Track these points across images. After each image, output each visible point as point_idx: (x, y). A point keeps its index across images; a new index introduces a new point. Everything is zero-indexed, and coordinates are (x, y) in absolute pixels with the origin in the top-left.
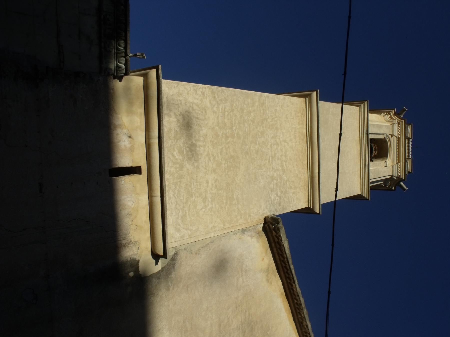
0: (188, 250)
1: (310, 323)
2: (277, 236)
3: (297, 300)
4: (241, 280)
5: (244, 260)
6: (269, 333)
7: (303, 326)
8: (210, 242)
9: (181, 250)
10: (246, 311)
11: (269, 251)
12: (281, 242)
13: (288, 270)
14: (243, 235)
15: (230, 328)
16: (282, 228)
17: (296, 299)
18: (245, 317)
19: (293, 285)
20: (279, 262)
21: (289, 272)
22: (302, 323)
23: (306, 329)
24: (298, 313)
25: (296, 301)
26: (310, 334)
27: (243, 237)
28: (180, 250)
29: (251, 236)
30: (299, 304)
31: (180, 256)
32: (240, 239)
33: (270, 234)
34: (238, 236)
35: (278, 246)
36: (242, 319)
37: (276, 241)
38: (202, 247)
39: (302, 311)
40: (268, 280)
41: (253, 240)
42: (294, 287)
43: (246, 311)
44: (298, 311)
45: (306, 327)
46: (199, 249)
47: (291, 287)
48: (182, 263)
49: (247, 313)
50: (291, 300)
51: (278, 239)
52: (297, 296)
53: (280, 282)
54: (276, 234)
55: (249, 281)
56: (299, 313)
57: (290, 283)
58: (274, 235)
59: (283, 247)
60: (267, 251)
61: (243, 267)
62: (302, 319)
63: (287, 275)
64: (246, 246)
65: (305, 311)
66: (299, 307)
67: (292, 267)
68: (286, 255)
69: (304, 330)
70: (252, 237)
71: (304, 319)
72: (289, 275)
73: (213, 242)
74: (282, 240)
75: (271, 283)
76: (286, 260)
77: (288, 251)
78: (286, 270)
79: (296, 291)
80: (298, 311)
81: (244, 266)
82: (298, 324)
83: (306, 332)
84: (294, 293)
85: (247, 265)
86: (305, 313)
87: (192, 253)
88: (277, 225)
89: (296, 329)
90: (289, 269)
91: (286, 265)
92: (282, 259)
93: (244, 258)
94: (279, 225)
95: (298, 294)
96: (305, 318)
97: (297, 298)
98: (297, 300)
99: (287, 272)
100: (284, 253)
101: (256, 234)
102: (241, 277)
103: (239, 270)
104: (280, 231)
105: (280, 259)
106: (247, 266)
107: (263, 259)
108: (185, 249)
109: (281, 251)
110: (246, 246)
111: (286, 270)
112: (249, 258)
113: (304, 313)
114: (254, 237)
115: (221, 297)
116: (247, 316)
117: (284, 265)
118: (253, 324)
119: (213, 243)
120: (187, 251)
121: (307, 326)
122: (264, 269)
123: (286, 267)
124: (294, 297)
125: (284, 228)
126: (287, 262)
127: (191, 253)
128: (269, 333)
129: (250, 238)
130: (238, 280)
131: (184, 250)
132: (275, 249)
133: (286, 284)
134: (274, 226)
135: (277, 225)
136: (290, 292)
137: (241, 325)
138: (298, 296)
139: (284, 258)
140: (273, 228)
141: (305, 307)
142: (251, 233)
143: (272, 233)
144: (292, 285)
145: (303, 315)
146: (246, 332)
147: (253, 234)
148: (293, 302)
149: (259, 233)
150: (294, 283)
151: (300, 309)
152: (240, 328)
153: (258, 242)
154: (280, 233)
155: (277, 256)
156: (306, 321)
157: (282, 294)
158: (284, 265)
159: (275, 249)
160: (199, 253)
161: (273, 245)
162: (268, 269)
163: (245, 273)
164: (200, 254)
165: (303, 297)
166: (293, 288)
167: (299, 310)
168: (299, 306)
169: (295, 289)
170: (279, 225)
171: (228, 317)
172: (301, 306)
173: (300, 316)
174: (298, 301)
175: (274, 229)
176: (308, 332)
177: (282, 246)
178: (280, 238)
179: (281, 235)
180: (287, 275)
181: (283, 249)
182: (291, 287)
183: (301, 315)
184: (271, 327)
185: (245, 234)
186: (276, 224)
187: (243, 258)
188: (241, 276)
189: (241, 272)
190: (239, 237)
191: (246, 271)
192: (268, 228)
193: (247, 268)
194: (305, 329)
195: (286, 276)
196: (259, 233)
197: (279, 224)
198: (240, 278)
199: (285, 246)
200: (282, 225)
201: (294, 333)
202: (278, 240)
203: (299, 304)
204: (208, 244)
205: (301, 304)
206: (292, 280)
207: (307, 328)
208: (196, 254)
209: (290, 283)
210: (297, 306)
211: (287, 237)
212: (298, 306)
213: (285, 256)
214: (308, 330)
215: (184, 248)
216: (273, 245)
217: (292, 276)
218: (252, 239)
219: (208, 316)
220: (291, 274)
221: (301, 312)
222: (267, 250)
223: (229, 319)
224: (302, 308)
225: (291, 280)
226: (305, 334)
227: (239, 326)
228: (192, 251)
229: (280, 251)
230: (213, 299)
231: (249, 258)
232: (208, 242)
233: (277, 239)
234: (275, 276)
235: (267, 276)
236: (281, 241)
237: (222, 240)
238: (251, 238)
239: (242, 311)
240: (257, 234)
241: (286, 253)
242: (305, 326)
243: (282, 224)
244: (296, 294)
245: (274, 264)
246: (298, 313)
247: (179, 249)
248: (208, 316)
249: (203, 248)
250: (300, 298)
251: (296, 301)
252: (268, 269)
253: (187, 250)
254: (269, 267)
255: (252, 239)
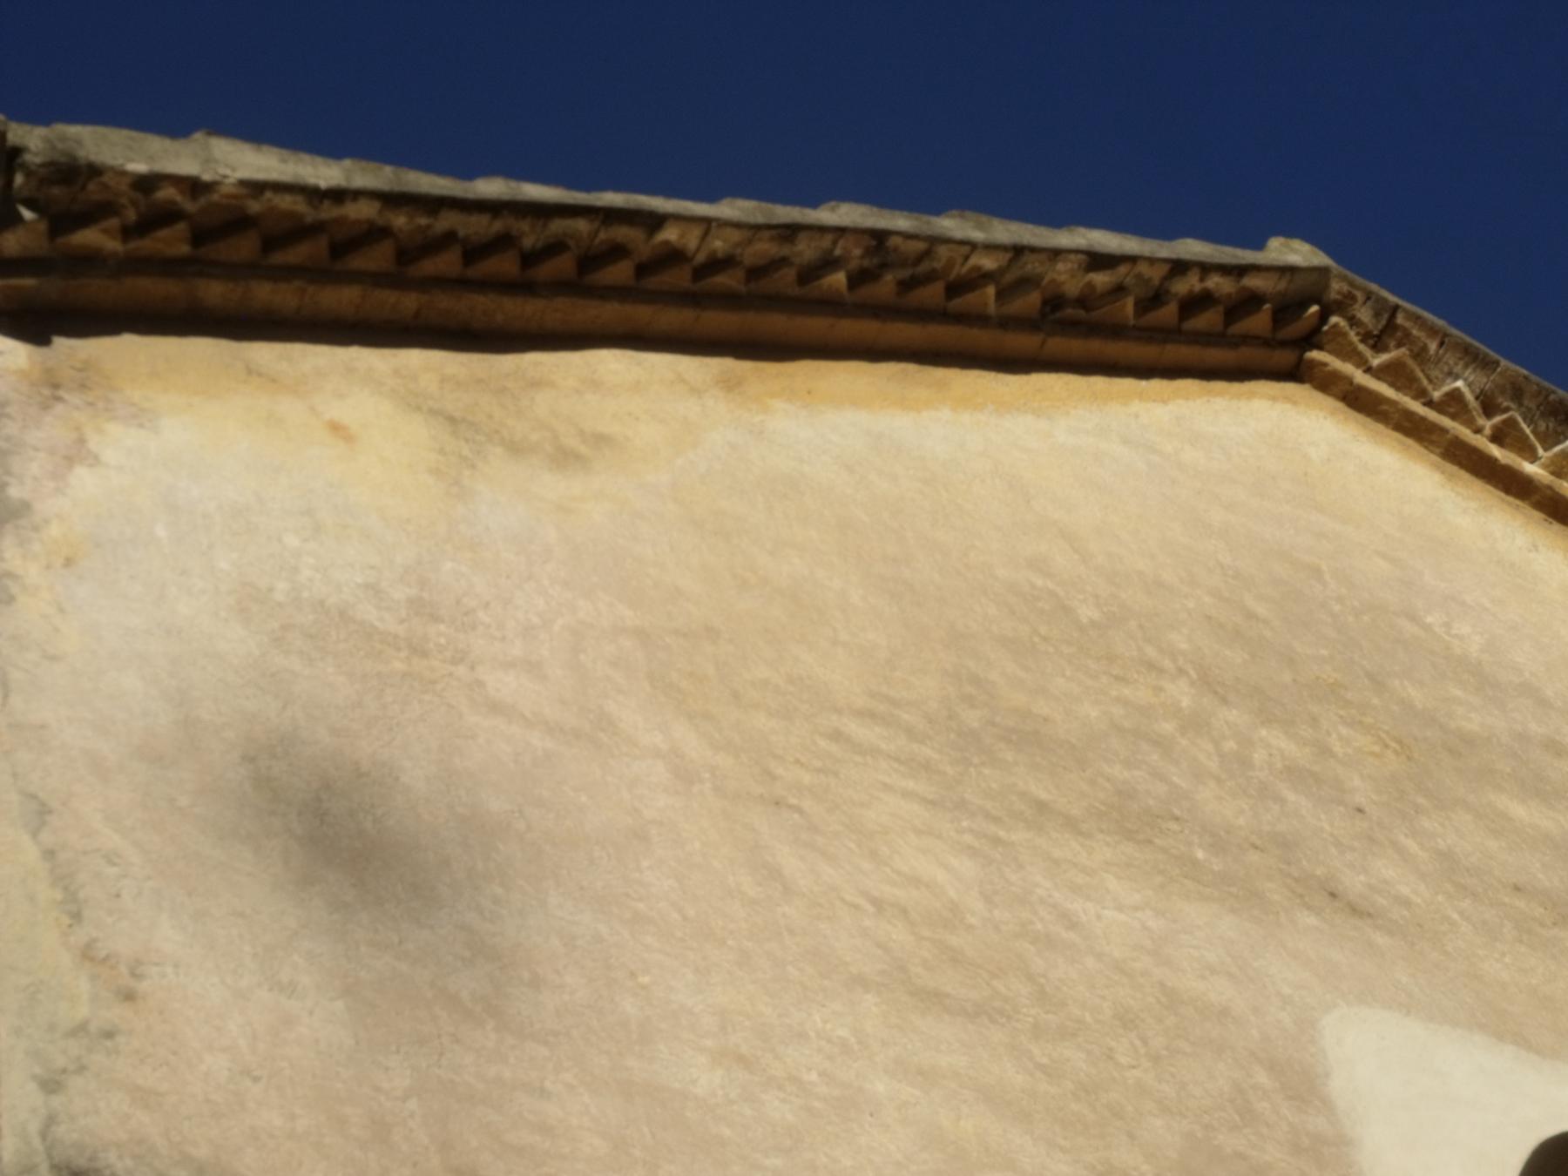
0: (61, 1062)
1: (1082, 230)
2: (131, 215)
3: (829, 263)
4: (504, 685)
5: (305, 594)
6: (1087, 613)
7: (1085, 300)
8: (35, 834)
9: (51, 1120)
10: (837, 736)
11: (264, 353)
12: (215, 197)
13: (504, 241)
14: (36, 529)
15: (972, 920)
16: (63, 139)
17: (809, 274)
18: (897, 760)
19: (667, 243)
20: (408, 303)
21: (530, 235)
22: (1055, 302)
23: (1128, 281)
24: (958, 304)
25: (838, 279)
26: (1179, 267)
27: (55, 530)
28: (44, 1135)
29: (70, 461)
30: (866, 263)
31: (112, 1157)
32: (69, 562)
33: (97, 289)
34: (32, 572)
35: (244, 247)
36: (907, 794)
37: (184, 249)
38: (66, 920)
39: (943, 251)
40: (564, 459)
41: (109, 455)
42: (690, 239)
43: (837, 736)
44: (932, 294)
45: (1101, 279)
46: (87, 954)
47: (678, 278)
48: (202, 1152)
49: (853, 728)
50: (815, 326)
51: (167, 216)
52: (785, 251)
53: (611, 363)
54: (114, 222)
55: (536, 620)
56: (956, 288)
57: (642, 270)
58: (113, 245)
59: (268, 194)
60: (260, 375)
61: (377, 624)
62: (1026, 283)
63: (563, 265)
64: (161, 532)
65: (951, 225)
66: (905, 274)
67: (490, 188)
68: (357, 194)
69: (1129, 305)
70: (77, 453)
71: (1031, 265)
72: (555, 248)
73: (43, 804)
74: (194, 186)
75: (600, 440)
76: (400, 221)
77: (325, 173)
78: (504, 265)
79: (735, 236)
80: (932, 294)
81: (368, 612)
82: (1058, 345)
83: (1156, 298)
84: (756, 272)
85: (367, 586)
86: (978, 235)
87: (109, 1035)
88: (29, 174)
89: (1099, 382)
90: (498, 226)
91: (450, 237)
92: (377, 258)
93: (282, 586)
94: (28, 157)
95: (769, 227)
96: (1018, 251)
97: (806, 250)
98: (829, 263)
99: (529, 259)
100: (328, 212)
101: (59, 408)
102: (472, 668)
103: (399, 666)
104: (95, 171)
105: (379, 280)
106: (373, 590)
107: (336, 428)
108: (51, 1085)
109: (300, 231)
110: (161, 532)
111: (504, 265)
112: (292, 541)
113: (973, 246)
114: (81, 441)
115: (641, 906)
116: (883, 746)
117: (447, 263)
118: (972, 718)
119: (50, 812)
120: (81, 1069)
121: (1098, 260)
122: (442, 451)
123: (475, 252)
124: (785, 280)
125: (74, 130)
126: (423, 221)
127: (109, 1043)
128: (1087, 613)
129: (83, 479)
130: (496, 708)
131: (57, 1101)
132: (265, 294)
133: (643, 314)
134: (27, 214)
135: (19, 179)
136: (730, 300)
137: (965, 824)
138: (790, 231)
139: (374, 233)
140: (43, 226)
141: (916, 215)
142: (36, 449)
143: (89, 261)
144: (674, 256)
145: (988, 263)
146: (1043, 796)
147: (51, 430)
148: (831, 305)
149: (56, 386)
150: (655, 221)
151: (924, 267)
152: (996, 841)
153: (140, 417)
154: (112, 169)
155: (341, 299)
156: (1056, 253)
157: (730, 385)
158: (447, 263)
159: (265, 294)
160: (123, 969)
161: (214, 292)
162: (452, 420)
163: (442, 627)
164: (139, 962)
165: (815, 204)
166: (701, 258)
167: (931, 277)
168: (884, 266)
169: (718, 245)
170: (28, 157)
171: (871, 909)
172: (894, 241)
173: (991, 290)
174: (838, 252)
175: (61, 221)
176: (1155, 274)
177: (254, 207)
178: (167, 193)
179: (139, 167)
180: (563, 265)
181: (286, 202)
182: (678, 278)
183: (981, 278)
184: (1039, 582)
185: (24, 508)
186: (9, 182)
187: (279, 596)
188: (461, 670)
189: (424, 654)
190: (48, 567)
191: (419, 607)
192: (29, 282)
193: (400, 593)
194: (1119, 290)
195: (562, 287)
196: (51, 387)
197: (17, 152)
198: (481, 684)
199: (261, 176)
200: (40, 131)
201: (1136, 406)
202: (181, 227)
203: (868, 252)
204: (49, 854)
205: (879, 237)
206: (622, 233)
207: (1123, 269)
208: (129, 996)
209: (642, 270)
210: (885, 287)
211: (177, 129)
212: (889, 278)
213: (363, 211)
214: (1143, 268)
215: (32, 1086)
216: (214, 292)
217: (582, 225)
218: (95, 461)
219: (814, 1077)
220: (558, 226)
221: (952, 276)
222: (249, 371)
223: (878, 903)
224: (921, 246)
225: (617, 252)
226: (1167, 313)
227: (968, 838)
228: (80, 1030)
229: (296, 254)
230: (644, 980)
231: (292, 541)
232: (31, 853)
233: (163, 233)
234: (536, 384)
235: (516, 449)
236: (202, 201)
237: (43, 727)
238: (91, 466)
239: (819, 771)
240: (59, 399)
241: (338, 195)
242: (1090, 285)
243: (27, 128)
244: (765, 248)
245: (415, 359)
246: (958, 304)
247: (37, 1143)
248: (814, 1077)
249: (77, 917)
250: (822, 229)
251: (838, 279)
252: (452, 420)
253: (64, 1071)
254: (433, 412)
255: (95, 461)
